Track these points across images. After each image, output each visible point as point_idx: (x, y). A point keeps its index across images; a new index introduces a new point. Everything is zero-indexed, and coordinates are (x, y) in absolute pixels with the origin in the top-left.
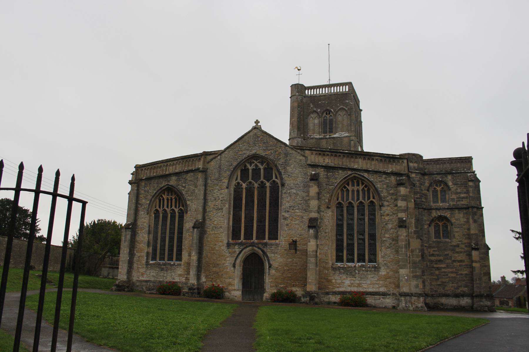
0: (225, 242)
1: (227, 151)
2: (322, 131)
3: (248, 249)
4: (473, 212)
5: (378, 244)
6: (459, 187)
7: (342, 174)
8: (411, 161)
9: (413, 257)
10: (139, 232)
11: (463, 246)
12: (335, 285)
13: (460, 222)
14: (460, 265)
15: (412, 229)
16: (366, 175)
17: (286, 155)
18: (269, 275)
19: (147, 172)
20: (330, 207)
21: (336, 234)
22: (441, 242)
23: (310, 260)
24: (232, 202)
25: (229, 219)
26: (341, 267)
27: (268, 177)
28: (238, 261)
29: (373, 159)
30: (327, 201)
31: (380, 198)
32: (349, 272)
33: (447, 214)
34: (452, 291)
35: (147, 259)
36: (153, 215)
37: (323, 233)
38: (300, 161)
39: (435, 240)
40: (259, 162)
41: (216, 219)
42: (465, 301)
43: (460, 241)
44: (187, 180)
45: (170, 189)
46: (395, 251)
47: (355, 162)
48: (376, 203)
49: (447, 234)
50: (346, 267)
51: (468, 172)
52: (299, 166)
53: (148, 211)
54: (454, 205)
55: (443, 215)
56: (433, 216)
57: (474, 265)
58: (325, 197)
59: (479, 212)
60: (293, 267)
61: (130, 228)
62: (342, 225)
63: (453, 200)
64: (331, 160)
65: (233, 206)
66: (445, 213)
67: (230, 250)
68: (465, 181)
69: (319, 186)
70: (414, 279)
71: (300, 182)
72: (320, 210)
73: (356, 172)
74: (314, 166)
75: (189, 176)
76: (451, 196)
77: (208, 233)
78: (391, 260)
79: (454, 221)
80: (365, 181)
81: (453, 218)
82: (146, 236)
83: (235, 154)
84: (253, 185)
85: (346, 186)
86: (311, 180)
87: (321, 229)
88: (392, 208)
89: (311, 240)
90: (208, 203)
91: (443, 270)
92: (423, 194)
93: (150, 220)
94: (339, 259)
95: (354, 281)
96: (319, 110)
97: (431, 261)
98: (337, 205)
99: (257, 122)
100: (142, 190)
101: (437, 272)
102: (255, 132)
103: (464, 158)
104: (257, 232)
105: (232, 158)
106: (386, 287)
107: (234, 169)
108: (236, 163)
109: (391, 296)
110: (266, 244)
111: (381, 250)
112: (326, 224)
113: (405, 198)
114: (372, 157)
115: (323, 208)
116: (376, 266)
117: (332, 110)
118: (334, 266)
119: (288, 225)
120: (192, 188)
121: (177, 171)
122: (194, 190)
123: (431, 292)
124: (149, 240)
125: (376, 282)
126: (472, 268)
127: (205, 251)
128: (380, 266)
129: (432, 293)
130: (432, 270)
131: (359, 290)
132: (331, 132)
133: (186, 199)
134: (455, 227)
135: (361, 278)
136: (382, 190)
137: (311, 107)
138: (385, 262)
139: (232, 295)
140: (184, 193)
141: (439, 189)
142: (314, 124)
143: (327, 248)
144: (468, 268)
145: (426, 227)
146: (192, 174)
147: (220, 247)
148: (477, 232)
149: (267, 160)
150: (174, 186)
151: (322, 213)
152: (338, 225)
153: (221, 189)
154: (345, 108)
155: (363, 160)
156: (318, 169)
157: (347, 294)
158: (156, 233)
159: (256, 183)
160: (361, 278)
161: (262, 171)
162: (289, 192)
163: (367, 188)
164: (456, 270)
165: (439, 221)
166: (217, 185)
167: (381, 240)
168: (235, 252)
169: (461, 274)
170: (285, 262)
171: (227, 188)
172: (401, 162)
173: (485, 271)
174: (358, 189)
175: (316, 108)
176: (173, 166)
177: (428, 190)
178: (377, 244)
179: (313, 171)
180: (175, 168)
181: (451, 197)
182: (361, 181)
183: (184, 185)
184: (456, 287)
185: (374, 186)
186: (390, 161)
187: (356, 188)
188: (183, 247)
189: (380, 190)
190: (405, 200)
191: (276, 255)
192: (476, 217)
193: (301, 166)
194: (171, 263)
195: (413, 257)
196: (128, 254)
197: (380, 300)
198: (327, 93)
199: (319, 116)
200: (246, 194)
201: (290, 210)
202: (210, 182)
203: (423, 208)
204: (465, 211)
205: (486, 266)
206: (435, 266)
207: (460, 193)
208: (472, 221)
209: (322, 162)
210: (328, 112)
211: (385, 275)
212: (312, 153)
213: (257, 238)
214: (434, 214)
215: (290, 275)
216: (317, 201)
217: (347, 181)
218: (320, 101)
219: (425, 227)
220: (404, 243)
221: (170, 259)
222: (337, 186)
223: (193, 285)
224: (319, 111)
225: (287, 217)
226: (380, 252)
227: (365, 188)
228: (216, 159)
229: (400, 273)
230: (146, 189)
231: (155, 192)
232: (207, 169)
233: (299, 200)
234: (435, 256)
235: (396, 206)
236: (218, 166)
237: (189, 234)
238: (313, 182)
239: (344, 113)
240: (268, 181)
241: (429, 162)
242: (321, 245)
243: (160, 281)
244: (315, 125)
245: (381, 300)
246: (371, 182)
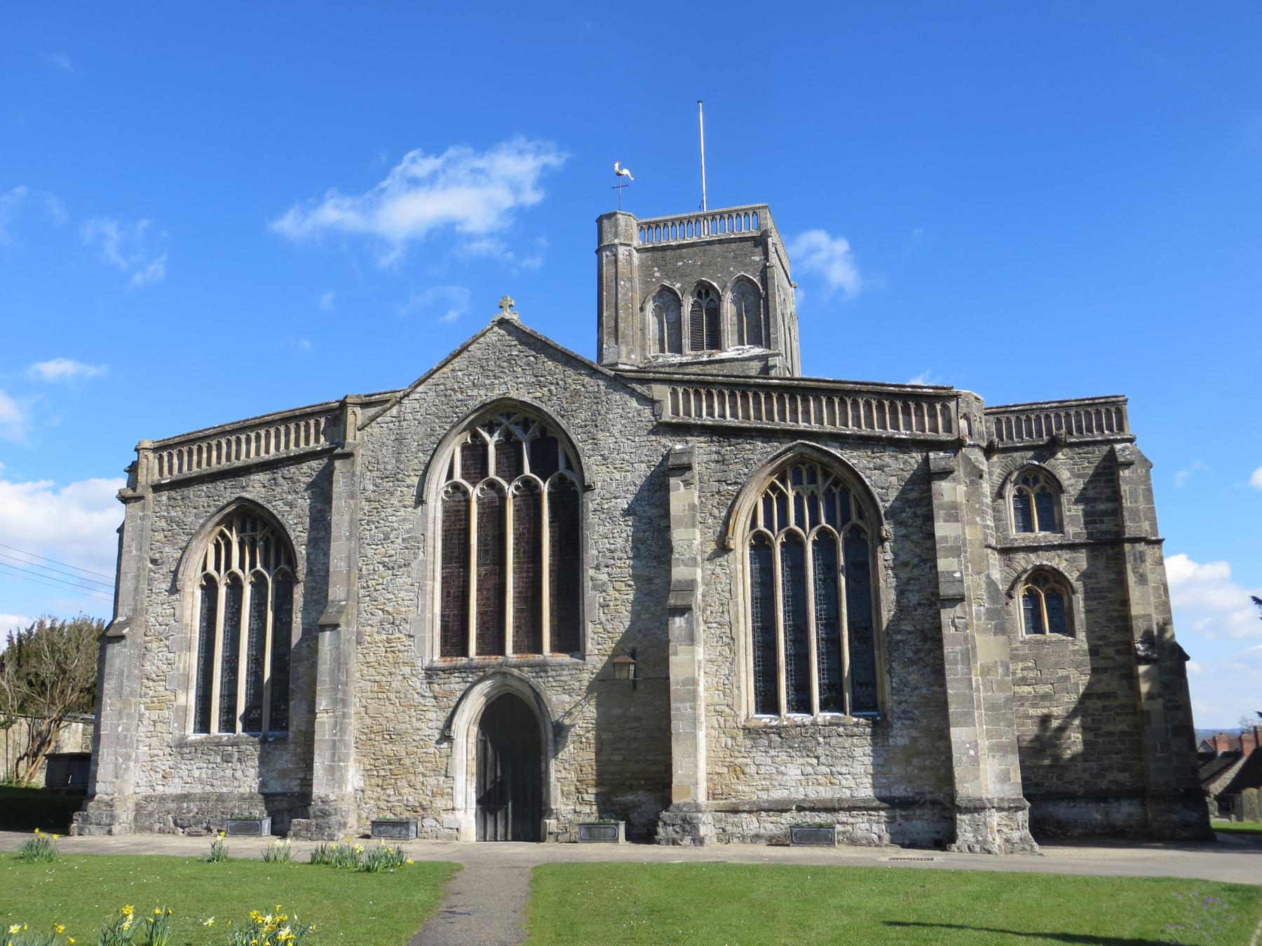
4: (1135, 554)
11: (1110, 651)
13: (1097, 583)
14: (1105, 708)
22: (1045, 642)
26: (771, 727)
39: (1028, 637)
40: (517, 424)
43: (1099, 639)
46: (933, 672)
48: (869, 532)
55: (1049, 564)
56: (1020, 569)
88: (916, 543)
94: (767, 703)
96: (678, 285)
103: (1103, 400)
106: (909, 782)
110: (542, 667)
111: (889, 672)
116: (878, 718)
117: (715, 284)
138: (904, 706)
144: (1127, 714)
154: (751, 277)
163: (839, 488)
167: (890, 642)
169: (1110, 734)
174: (812, 492)
175: (669, 278)
182: (821, 468)
184: (1095, 772)
188: (291, 686)
204: (1110, 552)
205: (1178, 708)
208: (1134, 579)
210: (703, 291)
211: (905, 747)
224: (679, 289)
226: (887, 677)
230: (173, 513)
237: (308, 646)
245: (897, 823)
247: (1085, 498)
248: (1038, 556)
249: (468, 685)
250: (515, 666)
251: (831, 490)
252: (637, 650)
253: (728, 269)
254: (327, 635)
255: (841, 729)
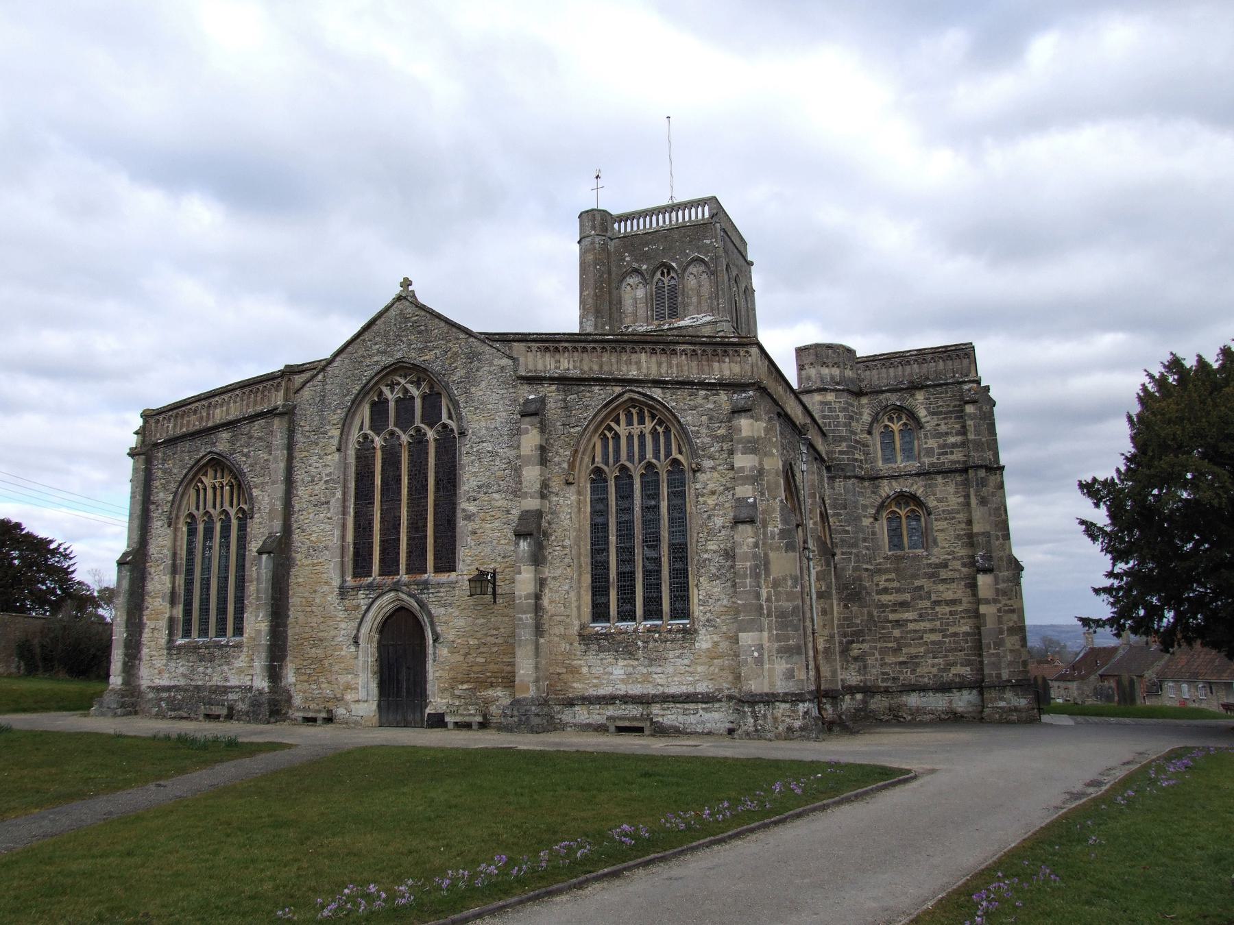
0: (336, 583)
1: (338, 359)
2: (652, 316)
3: (386, 597)
4: (977, 479)
5: (691, 570)
6: (944, 418)
7: (600, 395)
8: (824, 363)
9: (778, 600)
10: (152, 570)
11: (957, 564)
12: (588, 679)
15: (775, 527)
16: (657, 393)
17: (473, 356)
18: (434, 661)
19: (168, 427)
20: (571, 480)
21: (592, 549)
22: (903, 558)
23: (521, 619)
24: (352, 485)
25: (344, 526)
27: (431, 416)
28: (364, 630)
29: (674, 352)
30: (565, 465)
31: (694, 453)
32: (623, 647)
33: (917, 487)
34: (935, 676)
35: (171, 634)
36: (185, 529)
37: (558, 548)
38: (502, 372)
40: (412, 383)
41: (314, 528)
42: (963, 701)
44: (251, 438)
45: (218, 463)
47: (631, 364)
49: (925, 539)
50: (613, 633)
51: (964, 382)
52: (498, 383)
53: (169, 518)
54: (932, 464)
56: (884, 495)
57: (983, 609)
58: (560, 456)
59: (992, 478)
60: (488, 639)
61: (127, 563)
62: (606, 525)
63: (930, 452)
64: (574, 361)
65: (356, 494)
66: (912, 485)
67: (347, 602)
68: (958, 403)
69: (543, 429)
70: (781, 658)
71: (502, 423)
72: (550, 490)
73: (634, 388)
74: (533, 380)
75: (257, 428)
76: (926, 443)
77: (299, 563)
78: (722, 609)
79: (935, 503)
80: (657, 410)
81: (932, 497)
82: (167, 579)
83: (356, 365)
84: (399, 437)
85: (613, 424)
86: (524, 415)
87: (553, 538)
89: (522, 568)
90: (297, 490)
91: (911, 626)
92: (856, 441)
93: (175, 540)
94: (599, 613)
95: (634, 668)
97: (882, 606)
98: (592, 476)
99: (406, 283)
100: (159, 468)
101: (897, 633)
102: (401, 307)
103: (954, 348)
104: (409, 553)
105: (349, 377)
107: (353, 402)
108: (358, 388)
109: (723, 704)
110: (425, 585)
111: (697, 585)
112: (564, 524)
113: (753, 446)
114: (672, 347)
115: (556, 485)
117: (674, 265)
118: (586, 632)
119: (475, 533)
120: (263, 455)
121: (231, 418)
122: (266, 460)
123: (884, 680)
124: (173, 587)
125: (687, 668)
126: (977, 615)
127: (292, 609)
128: (696, 626)
129: (885, 684)
130: (884, 629)
131: (645, 692)
132: (674, 314)
133: (251, 484)
134: (936, 520)
135: (651, 660)
136: (697, 428)
137: (627, 261)
139: (353, 713)
140: (245, 470)
141: (896, 427)
142: (635, 299)
143: (567, 587)
144: (969, 617)
145: (867, 522)
146: (262, 422)
147: (325, 595)
148: (988, 528)
149: (428, 376)
150: (224, 455)
151: (555, 499)
152: (594, 526)
153: (326, 454)
155: (650, 357)
156: (543, 387)
157: (617, 702)
158: (190, 571)
159: (404, 433)
160: (651, 660)
161: (418, 403)
162: (477, 451)
164: (942, 624)
165: (898, 505)
166: (317, 444)
168: (358, 606)
169: (955, 634)
170: (470, 628)
171: (339, 450)
172: (742, 353)
173: (1011, 624)
175: (637, 260)
176: (222, 406)
177: (870, 433)
178: (690, 569)
179: (530, 392)
180: (227, 410)
181: (925, 446)
183: (245, 450)
185: (679, 422)
186: (715, 354)
187: (636, 429)
189: (693, 428)
190: (754, 451)
191: (450, 610)
192: (984, 492)
193: (503, 382)
194: (221, 641)
195: (778, 600)
196: (124, 625)
197: (698, 715)
198: (662, 227)
199: (646, 280)
200: (382, 463)
201: (480, 496)
202: (302, 439)
203: (856, 477)
205: (1013, 611)
206: (892, 617)
207: (947, 434)
209: (553, 367)
210: (665, 271)
212: (529, 347)
213: (409, 571)
214: (887, 489)
215: (484, 660)
216: (538, 467)
217: (611, 411)
218: (647, 244)
219: (864, 524)
220: (749, 564)
221: (222, 631)
222: (588, 426)
223: (261, 692)
224: (646, 270)
225: (474, 514)
226: (696, 591)
227: (658, 427)
228: (315, 382)
229: (740, 644)
231: (184, 472)
232: (295, 407)
233: (499, 470)
234: (892, 593)
235: (732, 468)
236: (318, 399)
238: (528, 419)
239: (702, 268)
240: (431, 425)
241: (870, 363)
242: (554, 578)
243: (197, 687)
244: (638, 302)
246: (671, 411)
247: (938, 433)
248: (899, 484)
249: (371, 600)
250: (405, 585)
251: (656, 430)
252: (497, 570)
253: (685, 251)
254: (1032, 667)
255: (657, 635)
